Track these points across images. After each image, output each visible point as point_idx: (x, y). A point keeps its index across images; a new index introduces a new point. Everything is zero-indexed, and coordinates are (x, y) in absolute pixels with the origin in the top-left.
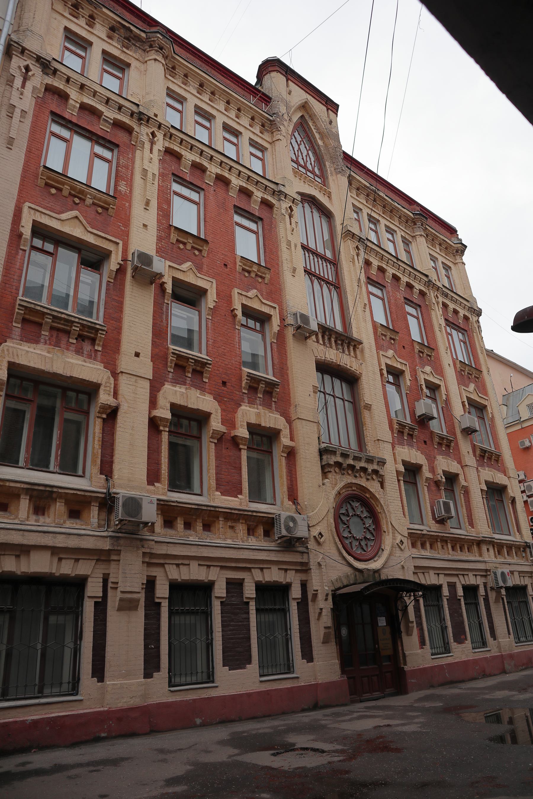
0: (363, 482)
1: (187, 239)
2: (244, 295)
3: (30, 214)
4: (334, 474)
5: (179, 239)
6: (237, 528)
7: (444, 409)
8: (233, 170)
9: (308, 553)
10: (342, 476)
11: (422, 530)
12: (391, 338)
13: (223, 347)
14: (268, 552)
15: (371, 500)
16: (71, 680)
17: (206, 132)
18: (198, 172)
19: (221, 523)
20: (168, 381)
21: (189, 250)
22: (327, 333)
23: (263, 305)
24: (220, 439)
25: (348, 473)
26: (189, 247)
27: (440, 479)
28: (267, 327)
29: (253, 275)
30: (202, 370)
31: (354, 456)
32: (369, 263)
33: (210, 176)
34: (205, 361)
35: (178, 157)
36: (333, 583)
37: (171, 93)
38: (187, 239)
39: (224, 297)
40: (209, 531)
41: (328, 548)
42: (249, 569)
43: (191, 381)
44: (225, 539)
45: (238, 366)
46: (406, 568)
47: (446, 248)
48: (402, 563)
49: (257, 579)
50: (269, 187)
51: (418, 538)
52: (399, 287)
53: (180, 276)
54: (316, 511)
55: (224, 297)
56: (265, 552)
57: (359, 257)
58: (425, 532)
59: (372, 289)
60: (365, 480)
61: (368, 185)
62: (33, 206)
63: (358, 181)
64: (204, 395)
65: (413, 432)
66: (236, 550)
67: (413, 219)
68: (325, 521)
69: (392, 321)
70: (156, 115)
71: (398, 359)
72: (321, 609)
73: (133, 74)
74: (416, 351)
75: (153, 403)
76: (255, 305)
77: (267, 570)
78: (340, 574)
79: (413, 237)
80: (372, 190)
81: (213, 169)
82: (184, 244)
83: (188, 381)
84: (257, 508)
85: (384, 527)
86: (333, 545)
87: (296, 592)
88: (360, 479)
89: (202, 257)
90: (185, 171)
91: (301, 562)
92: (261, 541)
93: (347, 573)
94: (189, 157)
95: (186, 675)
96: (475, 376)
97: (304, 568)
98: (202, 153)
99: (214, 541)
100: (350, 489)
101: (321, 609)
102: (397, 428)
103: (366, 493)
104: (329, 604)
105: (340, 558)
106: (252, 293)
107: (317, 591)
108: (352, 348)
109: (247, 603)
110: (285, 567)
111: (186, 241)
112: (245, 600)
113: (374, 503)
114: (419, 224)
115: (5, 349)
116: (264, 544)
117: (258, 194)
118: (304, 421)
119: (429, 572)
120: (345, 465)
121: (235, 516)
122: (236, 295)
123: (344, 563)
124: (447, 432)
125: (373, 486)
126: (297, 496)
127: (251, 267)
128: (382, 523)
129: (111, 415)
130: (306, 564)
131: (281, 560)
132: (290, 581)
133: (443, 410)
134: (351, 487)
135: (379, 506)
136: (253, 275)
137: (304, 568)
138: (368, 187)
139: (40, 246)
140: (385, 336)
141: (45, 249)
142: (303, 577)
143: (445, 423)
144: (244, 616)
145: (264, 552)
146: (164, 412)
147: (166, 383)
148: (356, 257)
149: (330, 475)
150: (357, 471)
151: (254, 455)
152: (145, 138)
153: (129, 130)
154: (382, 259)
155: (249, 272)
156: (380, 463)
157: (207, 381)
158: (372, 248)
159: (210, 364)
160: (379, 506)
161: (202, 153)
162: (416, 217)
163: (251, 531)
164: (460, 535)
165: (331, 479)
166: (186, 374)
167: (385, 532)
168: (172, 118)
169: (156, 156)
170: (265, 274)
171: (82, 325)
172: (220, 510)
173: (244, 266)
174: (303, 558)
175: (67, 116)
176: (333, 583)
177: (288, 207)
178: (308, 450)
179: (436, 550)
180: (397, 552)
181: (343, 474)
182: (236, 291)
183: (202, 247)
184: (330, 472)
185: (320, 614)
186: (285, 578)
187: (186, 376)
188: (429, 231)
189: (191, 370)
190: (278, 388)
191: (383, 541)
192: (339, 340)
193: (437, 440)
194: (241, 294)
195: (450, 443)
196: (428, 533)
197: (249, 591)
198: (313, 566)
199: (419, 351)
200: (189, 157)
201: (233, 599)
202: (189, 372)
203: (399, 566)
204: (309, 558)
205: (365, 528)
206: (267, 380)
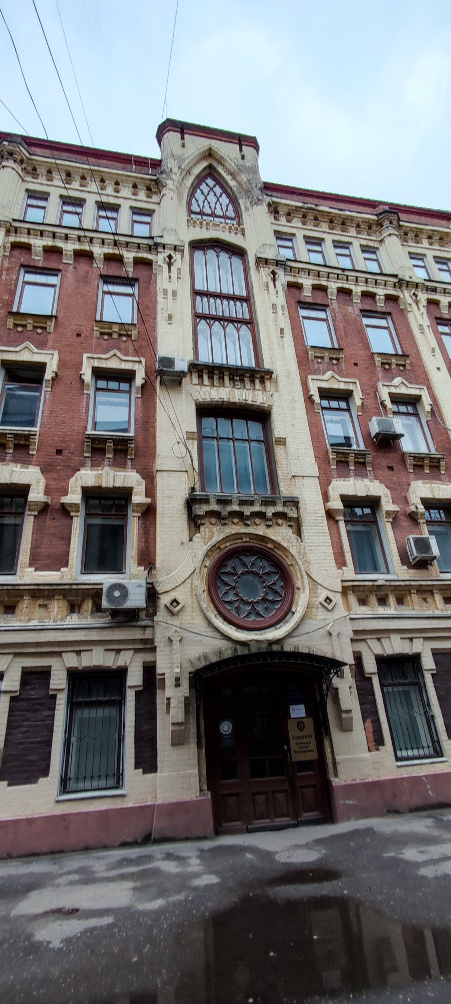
0: (260, 530)
1: (26, 321)
2: (96, 358)
3: (89, 362)
4: (210, 526)
5: (16, 322)
6: (51, 606)
7: (431, 423)
8: (95, 241)
9: (153, 627)
10: (223, 527)
11: (376, 581)
12: (331, 359)
13: (63, 416)
14: (87, 631)
15: (276, 550)
16: (116, 773)
17: (423, 270)
18: (55, 256)
19: (25, 603)
20: (333, 478)
21: (31, 331)
22: (216, 372)
23: (123, 363)
24: (44, 510)
25: (233, 522)
26: (30, 327)
27: (415, 510)
28: (419, 408)
29: (115, 336)
30: (27, 443)
31: (239, 500)
32: (300, 286)
33: (66, 255)
34: (27, 433)
35: (27, 248)
36: (192, 663)
37: (412, 256)
38: (26, 321)
39: (371, 391)
40: (13, 613)
41: (190, 618)
42: (59, 654)
43: (13, 456)
44: (29, 620)
45: (81, 431)
46: (334, 634)
47: (441, 239)
48: (328, 628)
49: (68, 665)
50: (142, 244)
51: (371, 592)
52: (352, 300)
53: (393, 390)
54: (174, 573)
55: (371, 391)
56: (82, 630)
57: (277, 282)
58: (380, 583)
59: (441, 329)
60: (264, 527)
61: (300, 204)
62: (90, 355)
63: (285, 205)
64: (27, 468)
65: (365, 458)
66: (36, 632)
67: (378, 221)
68: (188, 585)
69: (338, 340)
70: (411, 277)
71: (341, 379)
72: (169, 699)
73: (382, 253)
74: (378, 364)
75: (326, 498)
76: (403, 390)
77: (87, 653)
78: (206, 651)
79: (381, 241)
80: (307, 208)
81: (69, 247)
82: (24, 326)
83: (352, 473)
84: (90, 579)
85: (298, 584)
86: (199, 613)
87: (135, 678)
88: (255, 527)
89: (47, 334)
90: (38, 259)
91: (142, 640)
92: (87, 618)
93: (221, 648)
94: (38, 243)
95: (107, 776)
96: (397, 365)
97: (148, 646)
98: (54, 236)
99: (9, 625)
100: (240, 541)
101: (169, 699)
102: (333, 459)
103: (267, 543)
104: (185, 690)
105: (209, 629)
106: (397, 380)
107: (164, 674)
108: (257, 382)
109: (54, 697)
110: (77, 648)
111: (25, 323)
112: (51, 693)
113: (281, 554)
114: (386, 223)
115: (79, 478)
116: (89, 621)
117: (129, 256)
118: (165, 473)
119: (389, 638)
120: (269, 514)
121: (46, 593)
122: (381, 386)
123: (216, 635)
124: (436, 449)
125: (281, 534)
126: (154, 560)
127: (111, 328)
128: (295, 578)
129: (149, 513)
130: (152, 641)
131: (107, 639)
132: (123, 664)
133: (428, 425)
134: (242, 539)
135: (290, 557)
136: (115, 336)
137: (148, 646)
138: (301, 208)
139: (337, 406)
140: (322, 358)
141: (109, 388)
142: (148, 657)
143: (433, 439)
144: (370, 697)
145: (79, 631)
146: (336, 504)
147: (333, 480)
148: (271, 284)
149: (202, 529)
150: (248, 518)
151: (351, 528)
152: (409, 300)
153: (148, 264)
154: (319, 276)
155: (110, 335)
156: (288, 504)
157: (35, 453)
158: (299, 269)
159: (369, 454)
160: (290, 557)
161: (54, 236)
162: (380, 217)
163: (74, 608)
164: (363, 581)
165: (203, 533)
166: (7, 451)
167: (298, 589)
168: (420, 275)
169: (424, 310)
170: (131, 331)
171: (355, 454)
172: (22, 588)
173: (102, 330)
174: (144, 634)
175: (379, 309)
176: (192, 663)
177: (269, 272)
178: (168, 504)
179: (409, 606)
180: (320, 614)
181: (225, 524)
182: (85, 356)
183: (46, 323)
184: (204, 524)
185: (168, 705)
186: (80, 661)
187: (7, 453)
188: (407, 227)
189: (11, 446)
190: (133, 444)
191: (295, 602)
192: (236, 376)
193: (410, 462)
194: (93, 358)
195: (439, 463)
196: (388, 583)
197: (59, 681)
198: (159, 642)
199: (383, 364)
200: (38, 243)
201: (33, 692)
202: (9, 448)
203: (323, 632)
204: (154, 634)
205: (265, 587)
206: (114, 437)
